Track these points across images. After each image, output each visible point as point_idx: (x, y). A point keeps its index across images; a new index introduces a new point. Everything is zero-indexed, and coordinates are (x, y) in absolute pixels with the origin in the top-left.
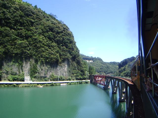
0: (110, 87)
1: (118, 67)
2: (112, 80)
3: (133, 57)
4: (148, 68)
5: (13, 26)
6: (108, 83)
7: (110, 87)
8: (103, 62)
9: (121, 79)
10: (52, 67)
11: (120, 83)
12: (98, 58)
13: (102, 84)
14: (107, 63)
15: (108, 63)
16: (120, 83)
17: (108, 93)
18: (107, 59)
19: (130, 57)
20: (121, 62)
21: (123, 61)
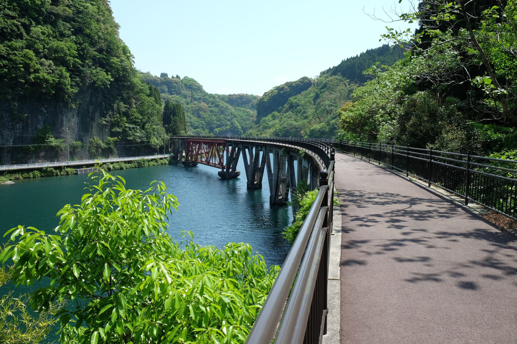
0: (240, 167)
1: (254, 113)
2: (247, 150)
3: (305, 78)
4: (309, 176)
5: (492, 103)
6: (233, 160)
7: (240, 167)
8: (206, 94)
9: (278, 144)
10: (289, 86)
11: (271, 156)
12: (186, 78)
13: (215, 166)
14: (219, 96)
15: (223, 98)
16: (271, 156)
17: (233, 191)
18: (218, 83)
19: (294, 77)
20: (265, 94)
21: (272, 91)
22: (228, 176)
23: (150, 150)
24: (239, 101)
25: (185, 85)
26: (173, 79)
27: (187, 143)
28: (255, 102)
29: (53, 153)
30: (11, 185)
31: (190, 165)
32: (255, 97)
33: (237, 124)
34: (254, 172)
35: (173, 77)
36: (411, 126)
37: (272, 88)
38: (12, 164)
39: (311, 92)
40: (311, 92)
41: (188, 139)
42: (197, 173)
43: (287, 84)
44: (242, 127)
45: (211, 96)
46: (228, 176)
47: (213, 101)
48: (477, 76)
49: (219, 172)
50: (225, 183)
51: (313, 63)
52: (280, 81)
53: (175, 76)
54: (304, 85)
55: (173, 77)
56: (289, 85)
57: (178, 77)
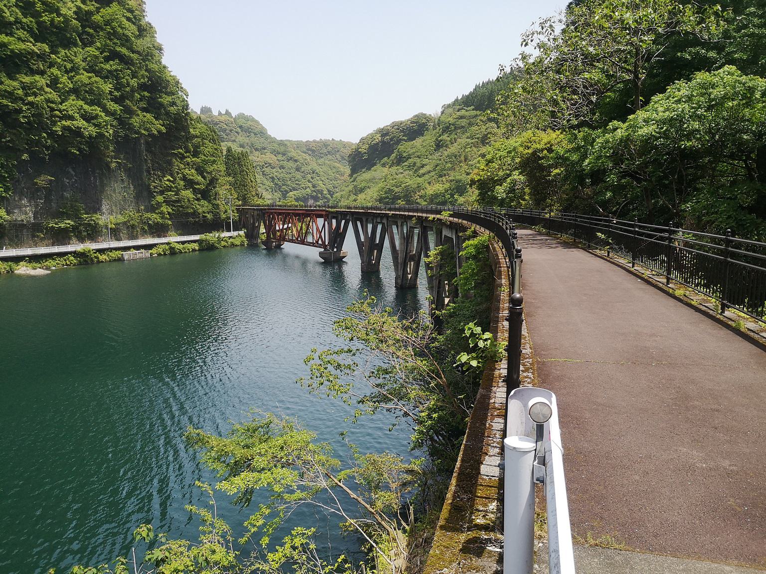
6: (338, 238)
8: (273, 141)
12: (241, 116)
15: (298, 145)
17: (338, 280)
19: (404, 114)
21: (372, 136)
22: (332, 261)
23: (218, 224)
24: (320, 150)
25: (241, 127)
26: (219, 117)
27: (268, 214)
28: (347, 152)
29: (93, 233)
30: (47, 275)
31: (273, 247)
32: (344, 145)
33: (321, 186)
34: (370, 251)
35: (220, 114)
36: (64, 128)
37: (371, 131)
38: (184, 235)
39: (428, 139)
40: (428, 139)
41: (269, 209)
42: (285, 257)
43: (393, 125)
44: (329, 191)
45: (282, 143)
46: (332, 261)
47: (282, 149)
48: (654, 94)
49: (320, 253)
50: (329, 269)
51: (431, 93)
52: (385, 122)
53: (223, 112)
54: (416, 128)
55: (220, 114)
56: (397, 126)
57: (228, 113)
